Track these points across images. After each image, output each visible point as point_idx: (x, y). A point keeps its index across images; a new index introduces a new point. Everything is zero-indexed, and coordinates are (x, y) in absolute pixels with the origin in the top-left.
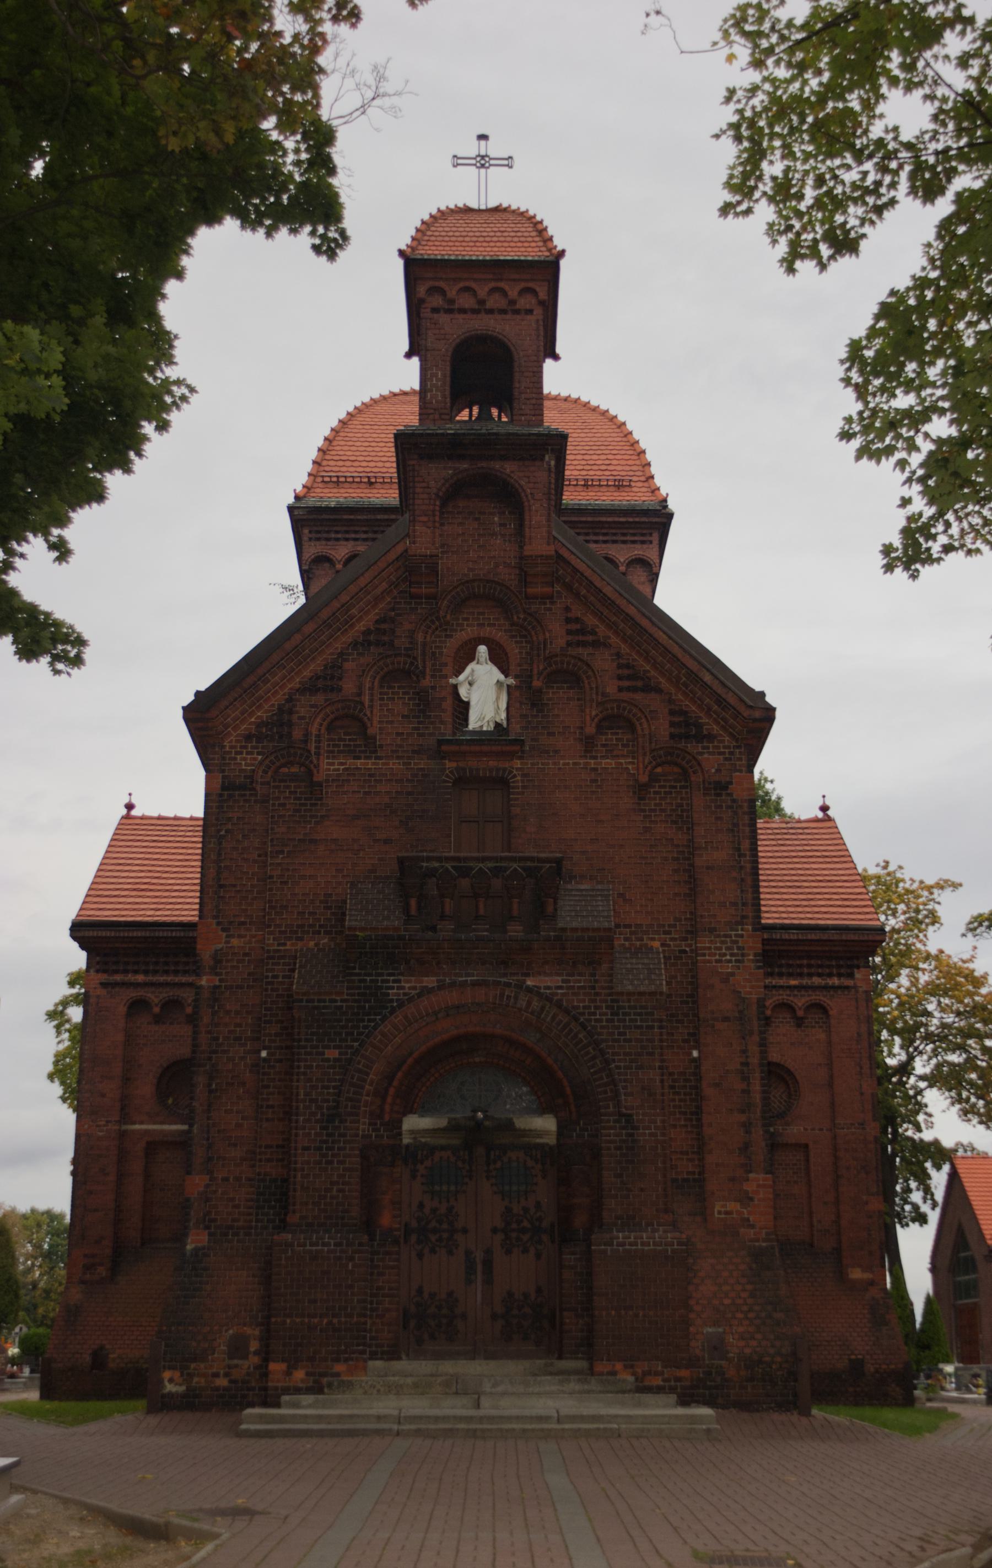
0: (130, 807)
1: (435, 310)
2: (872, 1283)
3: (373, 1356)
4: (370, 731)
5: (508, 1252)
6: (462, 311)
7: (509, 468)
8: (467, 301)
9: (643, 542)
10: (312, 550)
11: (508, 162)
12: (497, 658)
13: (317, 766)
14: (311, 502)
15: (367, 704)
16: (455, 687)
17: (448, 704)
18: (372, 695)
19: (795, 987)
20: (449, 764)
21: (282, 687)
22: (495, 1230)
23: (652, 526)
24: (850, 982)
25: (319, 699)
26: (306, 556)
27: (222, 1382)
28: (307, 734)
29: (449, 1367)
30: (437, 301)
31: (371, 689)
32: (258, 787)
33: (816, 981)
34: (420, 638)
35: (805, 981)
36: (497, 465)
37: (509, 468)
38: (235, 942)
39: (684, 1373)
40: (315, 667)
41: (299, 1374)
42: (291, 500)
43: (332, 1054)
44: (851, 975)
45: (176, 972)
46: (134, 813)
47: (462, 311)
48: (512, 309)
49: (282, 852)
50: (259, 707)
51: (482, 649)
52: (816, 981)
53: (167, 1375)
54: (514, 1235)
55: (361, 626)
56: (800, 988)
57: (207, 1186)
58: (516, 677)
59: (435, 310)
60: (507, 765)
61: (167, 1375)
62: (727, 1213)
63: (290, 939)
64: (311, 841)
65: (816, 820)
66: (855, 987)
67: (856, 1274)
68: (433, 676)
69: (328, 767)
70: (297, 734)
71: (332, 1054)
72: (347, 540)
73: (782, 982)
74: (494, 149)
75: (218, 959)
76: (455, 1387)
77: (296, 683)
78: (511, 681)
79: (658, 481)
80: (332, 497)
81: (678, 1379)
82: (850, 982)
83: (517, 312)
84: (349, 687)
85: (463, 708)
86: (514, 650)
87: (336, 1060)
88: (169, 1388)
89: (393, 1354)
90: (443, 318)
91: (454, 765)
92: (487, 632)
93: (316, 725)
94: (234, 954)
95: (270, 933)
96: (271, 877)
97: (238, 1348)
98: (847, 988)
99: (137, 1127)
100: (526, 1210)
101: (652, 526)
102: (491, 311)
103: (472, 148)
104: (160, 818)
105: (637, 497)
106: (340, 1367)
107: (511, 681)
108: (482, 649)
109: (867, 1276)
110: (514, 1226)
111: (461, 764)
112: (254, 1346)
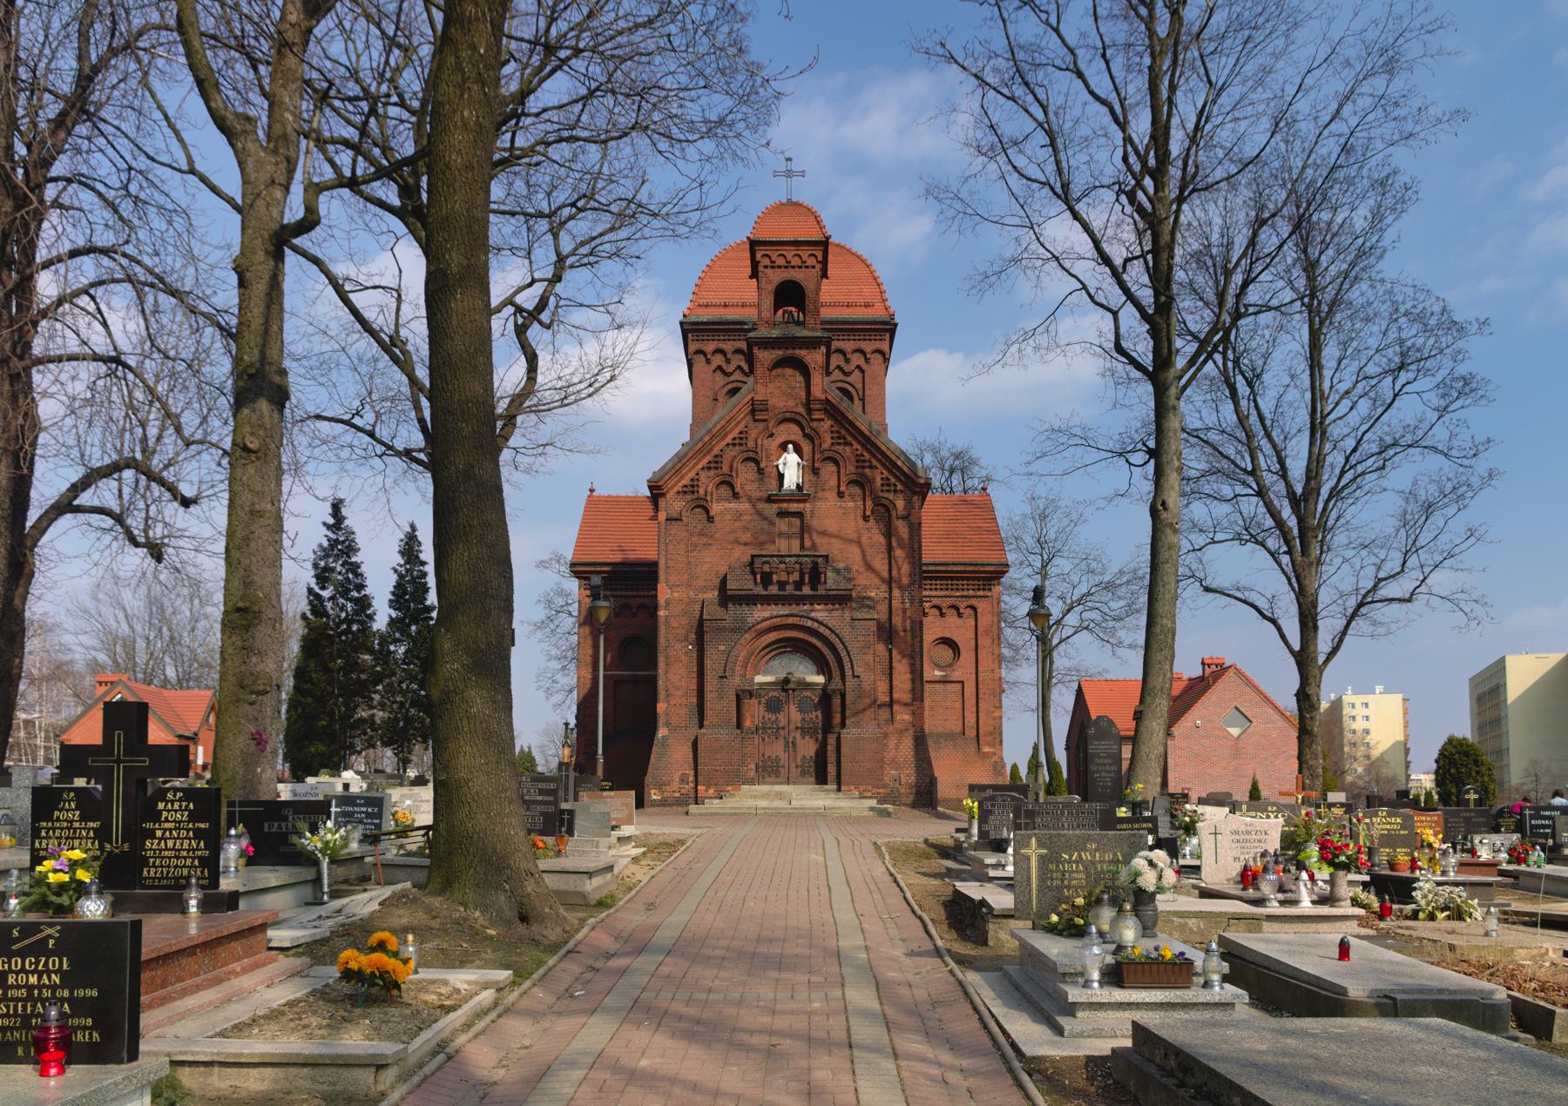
0: (592, 491)
1: (766, 267)
2: (994, 754)
3: (743, 783)
6: (779, 267)
7: (799, 352)
8: (781, 262)
10: (693, 347)
11: (803, 174)
12: (798, 450)
14: (693, 319)
17: (775, 472)
23: (886, 330)
25: (712, 473)
26: (690, 351)
27: (678, 795)
29: (777, 788)
30: (766, 261)
33: (971, 592)
34: (759, 442)
35: (965, 593)
36: (797, 352)
37: (799, 352)
38: (675, 594)
39: (881, 791)
41: (711, 791)
42: (681, 318)
43: (722, 648)
45: (627, 590)
47: (779, 267)
48: (804, 265)
51: (790, 446)
53: (653, 791)
55: (731, 436)
56: (962, 597)
59: (766, 267)
61: (653, 791)
67: (986, 749)
69: (716, 508)
70: (702, 491)
71: (722, 648)
74: (796, 166)
75: (667, 603)
76: (780, 796)
77: (700, 466)
79: (889, 303)
80: (705, 316)
83: (807, 267)
85: (781, 477)
86: (807, 448)
88: (654, 797)
89: (751, 782)
90: (769, 271)
92: (792, 438)
97: (683, 780)
101: (886, 330)
102: (793, 267)
103: (782, 166)
104: (609, 496)
105: (876, 313)
106: (729, 788)
108: (790, 446)
109: (992, 750)
112: (691, 778)
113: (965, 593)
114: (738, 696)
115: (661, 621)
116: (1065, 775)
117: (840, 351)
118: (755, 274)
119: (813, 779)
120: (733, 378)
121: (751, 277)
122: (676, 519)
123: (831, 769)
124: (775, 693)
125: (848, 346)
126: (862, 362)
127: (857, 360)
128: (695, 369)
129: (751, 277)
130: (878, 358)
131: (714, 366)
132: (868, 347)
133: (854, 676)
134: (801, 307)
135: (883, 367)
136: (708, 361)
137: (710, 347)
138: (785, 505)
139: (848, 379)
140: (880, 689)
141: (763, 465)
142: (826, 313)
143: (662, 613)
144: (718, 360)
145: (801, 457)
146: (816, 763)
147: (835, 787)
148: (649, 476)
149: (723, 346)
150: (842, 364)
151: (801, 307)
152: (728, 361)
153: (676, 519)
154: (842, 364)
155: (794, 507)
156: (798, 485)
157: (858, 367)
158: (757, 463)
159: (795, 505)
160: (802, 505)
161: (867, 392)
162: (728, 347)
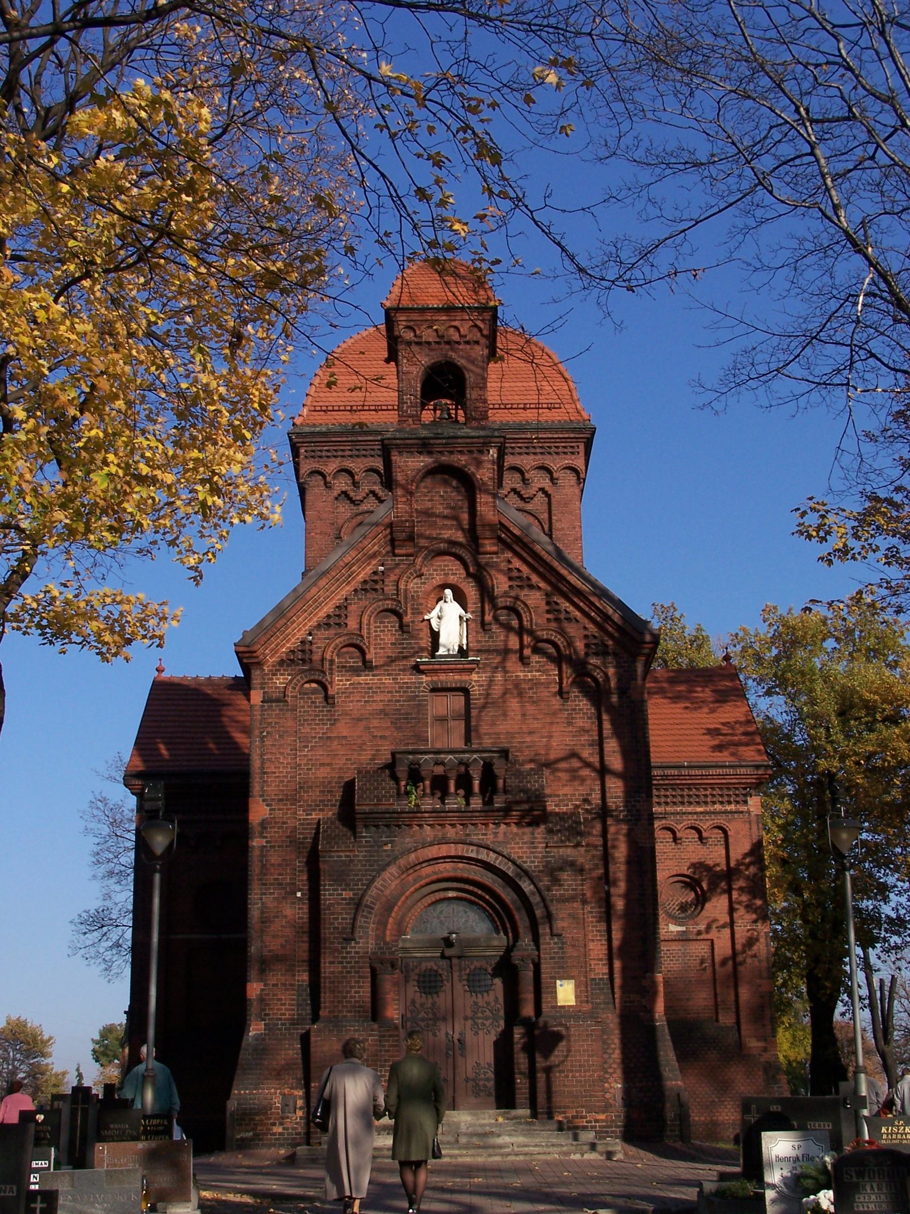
4: (368, 657)
5: (477, 1033)
9: (572, 453)
12: (460, 598)
13: (331, 683)
15: (365, 635)
16: (429, 620)
18: (369, 629)
19: (701, 813)
20: (424, 678)
21: (304, 626)
22: (466, 1018)
24: (745, 808)
26: (302, 472)
28: (323, 660)
30: (409, 336)
31: (369, 624)
32: (289, 699)
33: (718, 807)
34: (402, 586)
35: (710, 808)
39: (602, 1117)
40: (328, 608)
44: (746, 802)
46: (164, 675)
49: (307, 747)
50: (288, 641)
51: (448, 592)
52: (718, 807)
54: (480, 1021)
57: (262, 990)
58: (472, 612)
60: (467, 678)
62: (631, 1002)
63: (315, 810)
64: (328, 738)
65: (720, 667)
66: (749, 812)
68: (413, 614)
69: (339, 682)
70: (316, 657)
72: (335, 457)
73: (690, 809)
77: (314, 622)
78: (469, 616)
80: (325, 422)
81: (596, 1121)
82: (745, 808)
84: (352, 624)
85: (435, 636)
86: (471, 591)
87: (351, 899)
91: (429, 679)
92: (452, 579)
93: (329, 653)
94: (276, 823)
95: (300, 806)
96: (300, 765)
98: (742, 812)
99: (180, 936)
100: (488, 1003)
107: (469, 616)
110: (480, 1015)
111: (435, 678)
113: (710, 808)
114: (373, 971)
115: (255, 855)
116: (157, 877)
117: (515, 469)
118: (392, 357)
119: (493, 1099)
120: (364, 507)
121: (387, 361)
122: (278, 700)
123: (521, 1082)
124: (430, 965)
125: (527, 462)
126: (546, 483)
127: (540, 481)
128: (309, 497)
129: (387, 361)
130: (572, 477)
131: (335, 494)
132: (556, 463)
133: (552, 935)
134: (460, 399)
135: (577, 491)
136: (328, 486)
137: (331, 467)
138: (443, 677)
139: (529, 507)
140: (593, 955)
141: (407, 619)
142: (497, 417)
143: (256, 843)
144: (342, 484)
145: (464, 607)
146: (497, 1073)
147: (528, 1112)
148: (238, 638)
149: (349, 464)
150: (519, 486)
151: (460, 399)
152: (355, 484)
153: (278, 700)
154: (519, 486)
155: (453, 679)
156: (460, 647)
157: (542, 490)
158: (399, 616)
159: (503, 895)
160: (465, 677)
161: (556, 525)
162: (357, 466)
